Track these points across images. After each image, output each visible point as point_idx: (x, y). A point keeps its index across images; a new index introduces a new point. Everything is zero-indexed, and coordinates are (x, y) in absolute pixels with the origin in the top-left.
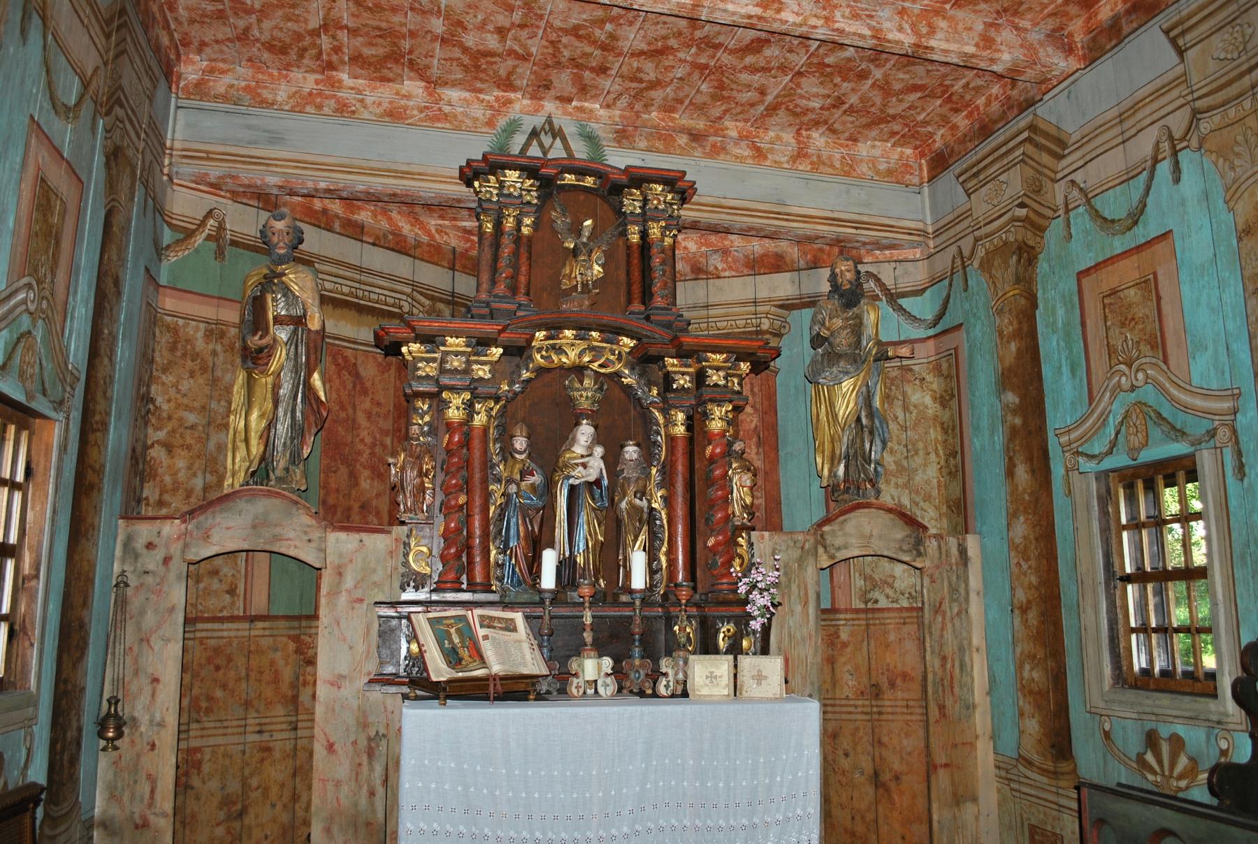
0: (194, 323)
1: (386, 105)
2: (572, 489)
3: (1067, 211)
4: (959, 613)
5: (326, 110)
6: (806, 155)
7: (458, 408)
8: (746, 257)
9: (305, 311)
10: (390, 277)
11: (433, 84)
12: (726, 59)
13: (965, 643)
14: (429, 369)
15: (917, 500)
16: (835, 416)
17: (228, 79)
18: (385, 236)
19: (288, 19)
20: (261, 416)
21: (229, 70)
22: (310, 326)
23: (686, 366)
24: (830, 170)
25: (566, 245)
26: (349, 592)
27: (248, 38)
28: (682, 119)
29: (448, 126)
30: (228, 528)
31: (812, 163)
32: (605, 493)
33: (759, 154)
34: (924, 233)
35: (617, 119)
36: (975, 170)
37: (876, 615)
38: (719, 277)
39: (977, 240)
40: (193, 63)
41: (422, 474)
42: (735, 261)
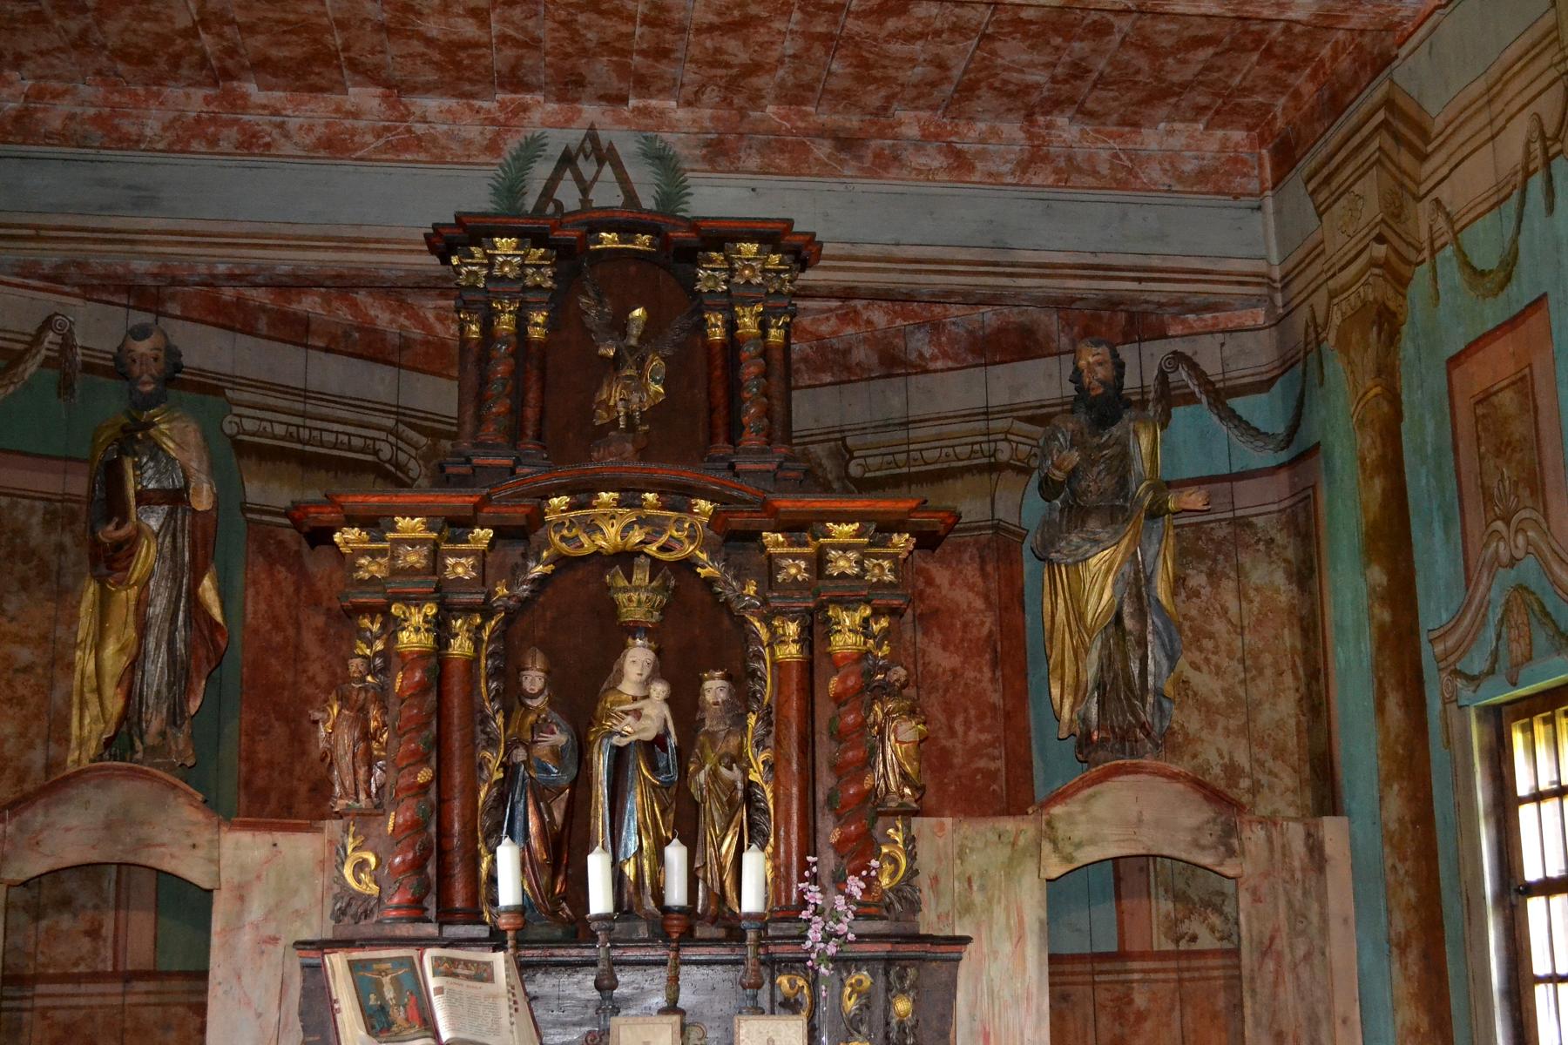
0: (26, 502)
1: (320, 130)
2: (619, 757)
3: (1433, 253)
4: (1308, 957)
5: (224, 145)
6: (1046, 158)
7: (417, 630)
8: (971, 333)
9: (186, 478)
10: (358, 404)
11: (397, 90)
12: (853, 25)
13: (1321, 1009)
14: (370, 568)
15: (1262, 756)
16: (1080, 617)
17: (65, 106)
18: (347, 335)
19: (141, 17)
20: (122, 650)
21: (66, 92)
22: (195, 504)
23: (800, 545)
24: (1091, 181)
25: (602, 351)
26: (256, 927)
27: (87, 44)
28: (821, 115)
29: (422, 156)
30: (68, 830)
31: (1057, 171)
32: (672, 758)
33: (960, 162)
34: (1265, 280)
35: (708, 124)
36: (1325, 172)
37: (1195, 963)
38: (926, 371)
39: (1332, 295)
40: (11, 84)
41: (367, 736)
42: (953, 341)
